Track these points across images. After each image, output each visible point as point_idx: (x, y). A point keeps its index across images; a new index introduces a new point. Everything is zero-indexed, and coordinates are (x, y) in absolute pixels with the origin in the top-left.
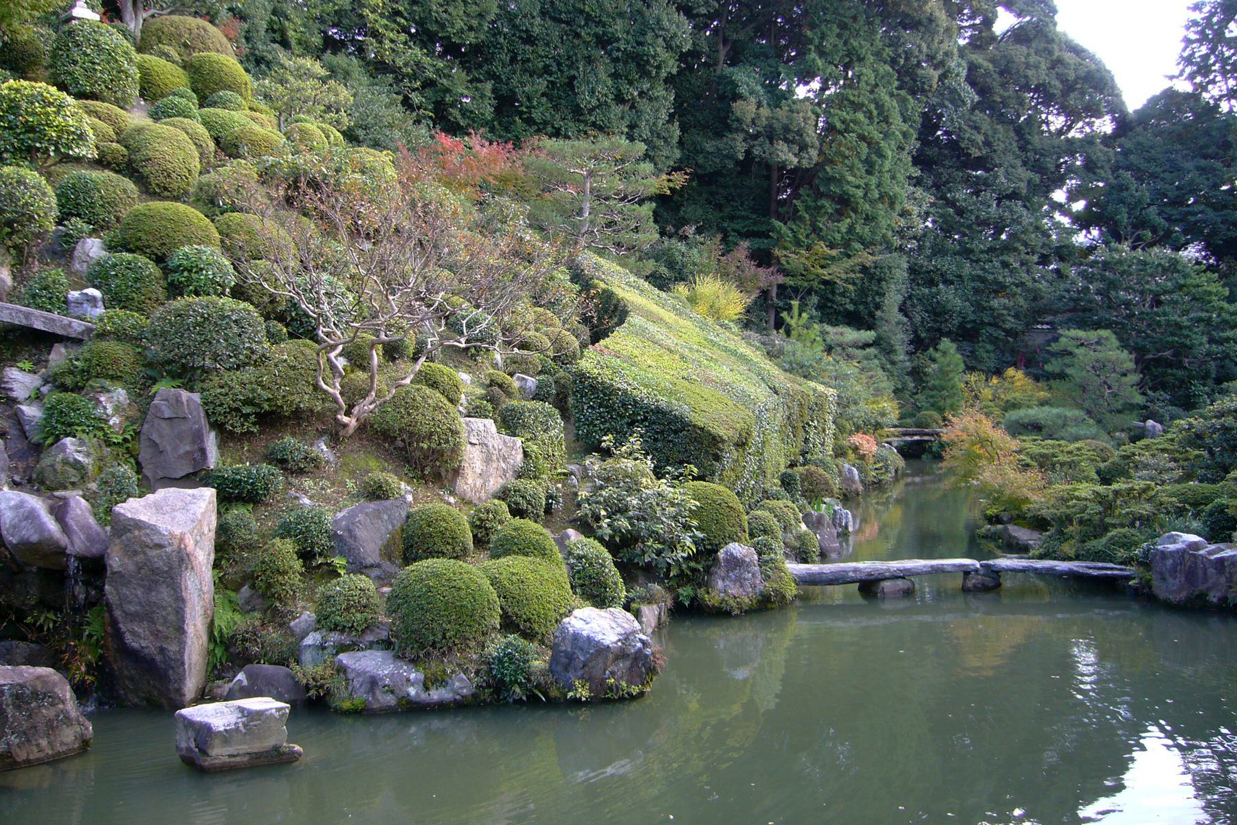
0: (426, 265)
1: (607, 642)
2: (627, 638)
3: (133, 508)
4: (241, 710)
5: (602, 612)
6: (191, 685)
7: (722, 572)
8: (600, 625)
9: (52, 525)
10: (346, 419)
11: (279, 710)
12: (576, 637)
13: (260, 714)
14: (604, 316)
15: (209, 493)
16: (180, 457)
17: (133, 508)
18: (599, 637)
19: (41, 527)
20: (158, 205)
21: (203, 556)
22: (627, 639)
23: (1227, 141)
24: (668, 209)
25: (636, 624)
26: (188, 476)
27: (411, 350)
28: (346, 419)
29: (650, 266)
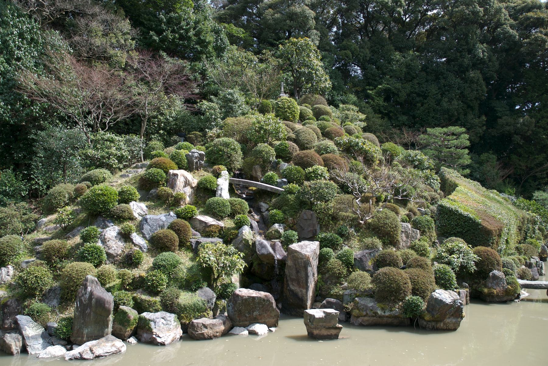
0: (197, 23)
1: (447, 302)
2: (454, 301)
3: (295, 246)
4: (324, 312)
5: (446, 292)
6: (309, 303)
7: (491, 280)
8: (446, 296)
9: (271, 250)
10: (361, 222)
11: (335, 313)
12: (436, 299)
13: (330, 313)
14: (448, 188)
15: (317, 243)
16: (309, 231)
17: (295, 246)
18: (444, 300)
19: (268, 250)
20: (305, 151)
21: (315, 263)
22: (454, 302)
23: (218, 93)
24: (153, 57)
25: (458, 297)
26: (311, 237)
27: (383, 200)
28: (361, 222)
29: (468, 171)
